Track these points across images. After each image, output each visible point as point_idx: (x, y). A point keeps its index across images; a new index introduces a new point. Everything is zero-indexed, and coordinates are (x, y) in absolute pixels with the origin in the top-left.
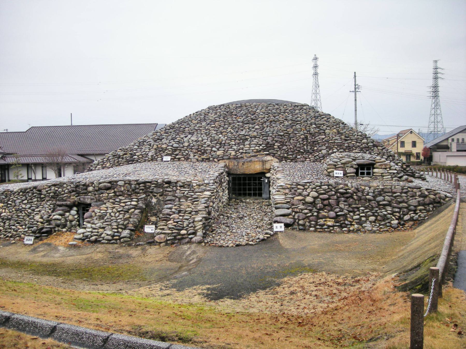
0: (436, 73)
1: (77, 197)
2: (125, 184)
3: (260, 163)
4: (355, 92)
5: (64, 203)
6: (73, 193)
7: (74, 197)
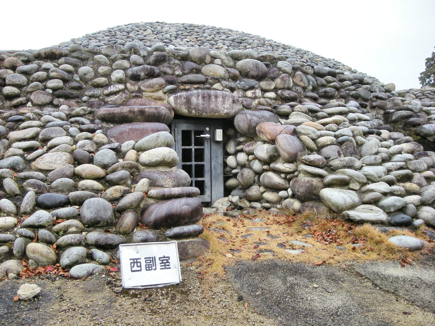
1: (172, 92)
2: (295, 69)
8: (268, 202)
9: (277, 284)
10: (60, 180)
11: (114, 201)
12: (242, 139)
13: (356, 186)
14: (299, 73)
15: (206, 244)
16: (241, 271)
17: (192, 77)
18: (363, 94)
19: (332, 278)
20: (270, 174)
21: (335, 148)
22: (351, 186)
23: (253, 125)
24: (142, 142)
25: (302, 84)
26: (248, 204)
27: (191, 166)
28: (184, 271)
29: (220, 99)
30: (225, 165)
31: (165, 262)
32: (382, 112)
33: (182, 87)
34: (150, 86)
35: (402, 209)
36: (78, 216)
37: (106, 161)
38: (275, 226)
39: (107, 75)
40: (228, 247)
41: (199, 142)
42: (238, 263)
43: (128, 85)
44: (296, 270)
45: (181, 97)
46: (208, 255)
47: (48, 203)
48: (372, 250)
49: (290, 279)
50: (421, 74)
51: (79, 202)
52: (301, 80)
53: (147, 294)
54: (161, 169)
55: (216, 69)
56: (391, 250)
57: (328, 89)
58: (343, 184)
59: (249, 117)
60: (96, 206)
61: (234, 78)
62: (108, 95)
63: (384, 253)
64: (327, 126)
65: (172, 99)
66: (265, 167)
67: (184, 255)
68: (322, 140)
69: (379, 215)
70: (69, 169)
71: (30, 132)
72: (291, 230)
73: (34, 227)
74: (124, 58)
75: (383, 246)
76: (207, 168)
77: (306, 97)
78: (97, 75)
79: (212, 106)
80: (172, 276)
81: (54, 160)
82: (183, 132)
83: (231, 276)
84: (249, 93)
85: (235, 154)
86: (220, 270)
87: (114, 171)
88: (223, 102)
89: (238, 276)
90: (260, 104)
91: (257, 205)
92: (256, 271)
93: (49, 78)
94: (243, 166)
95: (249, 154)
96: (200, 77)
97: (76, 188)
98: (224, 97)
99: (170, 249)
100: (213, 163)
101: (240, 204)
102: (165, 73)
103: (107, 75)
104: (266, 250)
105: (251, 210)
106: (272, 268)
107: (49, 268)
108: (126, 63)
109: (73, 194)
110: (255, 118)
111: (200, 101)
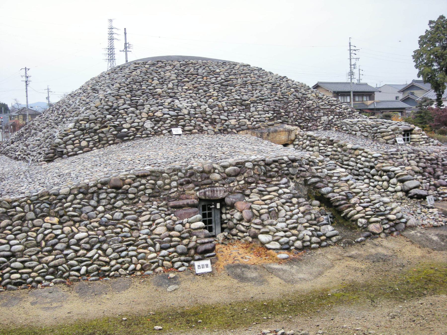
0: (111, 34)
1: (198, 190)
2: (254, 165)
3: (286, 133)
4: (126, 51)
5: (185, 202)
6: (191, 185)
7: (193, 192)
8: (240, 237)
9: (239, 271)
10: (166, 238)
11: (186, 245)
12: (228, 208)
13: (272, 233)
14: (257, 167)
15: (217, 258)
16: (229, 267)
17: (205, 182)
18: (291, 172)
19: (255, 269)
20: (240, 226)
21: (266, 215)
22: (270, 233)
23: (233, 202)
24: (190, 220)
25: (258, 173)
26: (231, 237)
27: (206, 220)
28: (212, 268)
29: (219, 192)
30: (221, 218)
31: (207, 266)
32: (303, 179)
33: (202, 187)
34: (188, 189)
35: (288, 243)
36: (175, 252)
37: (180, 229)
38: (241, 250)
39: (169, 184)
40: (224, 259)
41: (210, 209)
42: (228, 265)
43: (179, 189)
44: (245, 266)
45: (202, 192)
46: (218, 262)
47: (165, 247)
48: (271, 259)
49: (243, 269)
50: (415, 52)
51: (175, 246)
52: (258, 171)
53: (203, 275)
54: (199, 231)
55: (216, 176)
56: (277, 259)
57: (272, 173)
58: (267, 233)
59: (231, 199)
60: (181, 248)
61: (224, 179)
62: (171, 193)
63: (275, 260)
64: (266, 202)
65: (198, 193)
66: (238, 222)
67: (212, 263)
68: (262, 211)
69: (277, 246)
70: (167, 233)
71: (147, 217)
72: (246, 251)
73: (163, 256)
74: (175, 175)
75: (274, 258)
76: (213, 220)
77: (260, 179)
78: (165, 184)
79: (215, 195)
80: (209, 269)
81: (161, 230)
82: (203, 206)
83: (226, 269)
84: (231, 185)
85: (226, 213)
86: (222, 267)
87: (183, 233)
88: (220, 193)
89: (228, 269)
90: (236, 189)
91: (235, 238)
92: (233, 267)
93: (146, 189)
94: (229, 220)
95: (232, 215)
96: (209, 181)
97: (171, 241)
98: (220, 191)
99: (208, 262)
100: (216, 218)
101: (228, 237)
102: (194, 181)
103: (169, 184)
104: (237, 260)
105: (233, 241)
106: (238, 266)
107: (172, 269)
108: (176, 177)
109: (172, 244)
110: (234, 200)
111: (210, 193)
